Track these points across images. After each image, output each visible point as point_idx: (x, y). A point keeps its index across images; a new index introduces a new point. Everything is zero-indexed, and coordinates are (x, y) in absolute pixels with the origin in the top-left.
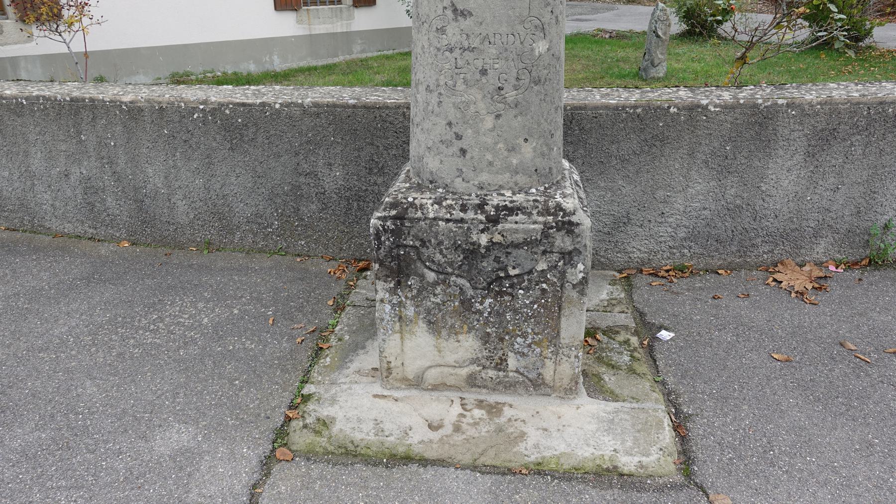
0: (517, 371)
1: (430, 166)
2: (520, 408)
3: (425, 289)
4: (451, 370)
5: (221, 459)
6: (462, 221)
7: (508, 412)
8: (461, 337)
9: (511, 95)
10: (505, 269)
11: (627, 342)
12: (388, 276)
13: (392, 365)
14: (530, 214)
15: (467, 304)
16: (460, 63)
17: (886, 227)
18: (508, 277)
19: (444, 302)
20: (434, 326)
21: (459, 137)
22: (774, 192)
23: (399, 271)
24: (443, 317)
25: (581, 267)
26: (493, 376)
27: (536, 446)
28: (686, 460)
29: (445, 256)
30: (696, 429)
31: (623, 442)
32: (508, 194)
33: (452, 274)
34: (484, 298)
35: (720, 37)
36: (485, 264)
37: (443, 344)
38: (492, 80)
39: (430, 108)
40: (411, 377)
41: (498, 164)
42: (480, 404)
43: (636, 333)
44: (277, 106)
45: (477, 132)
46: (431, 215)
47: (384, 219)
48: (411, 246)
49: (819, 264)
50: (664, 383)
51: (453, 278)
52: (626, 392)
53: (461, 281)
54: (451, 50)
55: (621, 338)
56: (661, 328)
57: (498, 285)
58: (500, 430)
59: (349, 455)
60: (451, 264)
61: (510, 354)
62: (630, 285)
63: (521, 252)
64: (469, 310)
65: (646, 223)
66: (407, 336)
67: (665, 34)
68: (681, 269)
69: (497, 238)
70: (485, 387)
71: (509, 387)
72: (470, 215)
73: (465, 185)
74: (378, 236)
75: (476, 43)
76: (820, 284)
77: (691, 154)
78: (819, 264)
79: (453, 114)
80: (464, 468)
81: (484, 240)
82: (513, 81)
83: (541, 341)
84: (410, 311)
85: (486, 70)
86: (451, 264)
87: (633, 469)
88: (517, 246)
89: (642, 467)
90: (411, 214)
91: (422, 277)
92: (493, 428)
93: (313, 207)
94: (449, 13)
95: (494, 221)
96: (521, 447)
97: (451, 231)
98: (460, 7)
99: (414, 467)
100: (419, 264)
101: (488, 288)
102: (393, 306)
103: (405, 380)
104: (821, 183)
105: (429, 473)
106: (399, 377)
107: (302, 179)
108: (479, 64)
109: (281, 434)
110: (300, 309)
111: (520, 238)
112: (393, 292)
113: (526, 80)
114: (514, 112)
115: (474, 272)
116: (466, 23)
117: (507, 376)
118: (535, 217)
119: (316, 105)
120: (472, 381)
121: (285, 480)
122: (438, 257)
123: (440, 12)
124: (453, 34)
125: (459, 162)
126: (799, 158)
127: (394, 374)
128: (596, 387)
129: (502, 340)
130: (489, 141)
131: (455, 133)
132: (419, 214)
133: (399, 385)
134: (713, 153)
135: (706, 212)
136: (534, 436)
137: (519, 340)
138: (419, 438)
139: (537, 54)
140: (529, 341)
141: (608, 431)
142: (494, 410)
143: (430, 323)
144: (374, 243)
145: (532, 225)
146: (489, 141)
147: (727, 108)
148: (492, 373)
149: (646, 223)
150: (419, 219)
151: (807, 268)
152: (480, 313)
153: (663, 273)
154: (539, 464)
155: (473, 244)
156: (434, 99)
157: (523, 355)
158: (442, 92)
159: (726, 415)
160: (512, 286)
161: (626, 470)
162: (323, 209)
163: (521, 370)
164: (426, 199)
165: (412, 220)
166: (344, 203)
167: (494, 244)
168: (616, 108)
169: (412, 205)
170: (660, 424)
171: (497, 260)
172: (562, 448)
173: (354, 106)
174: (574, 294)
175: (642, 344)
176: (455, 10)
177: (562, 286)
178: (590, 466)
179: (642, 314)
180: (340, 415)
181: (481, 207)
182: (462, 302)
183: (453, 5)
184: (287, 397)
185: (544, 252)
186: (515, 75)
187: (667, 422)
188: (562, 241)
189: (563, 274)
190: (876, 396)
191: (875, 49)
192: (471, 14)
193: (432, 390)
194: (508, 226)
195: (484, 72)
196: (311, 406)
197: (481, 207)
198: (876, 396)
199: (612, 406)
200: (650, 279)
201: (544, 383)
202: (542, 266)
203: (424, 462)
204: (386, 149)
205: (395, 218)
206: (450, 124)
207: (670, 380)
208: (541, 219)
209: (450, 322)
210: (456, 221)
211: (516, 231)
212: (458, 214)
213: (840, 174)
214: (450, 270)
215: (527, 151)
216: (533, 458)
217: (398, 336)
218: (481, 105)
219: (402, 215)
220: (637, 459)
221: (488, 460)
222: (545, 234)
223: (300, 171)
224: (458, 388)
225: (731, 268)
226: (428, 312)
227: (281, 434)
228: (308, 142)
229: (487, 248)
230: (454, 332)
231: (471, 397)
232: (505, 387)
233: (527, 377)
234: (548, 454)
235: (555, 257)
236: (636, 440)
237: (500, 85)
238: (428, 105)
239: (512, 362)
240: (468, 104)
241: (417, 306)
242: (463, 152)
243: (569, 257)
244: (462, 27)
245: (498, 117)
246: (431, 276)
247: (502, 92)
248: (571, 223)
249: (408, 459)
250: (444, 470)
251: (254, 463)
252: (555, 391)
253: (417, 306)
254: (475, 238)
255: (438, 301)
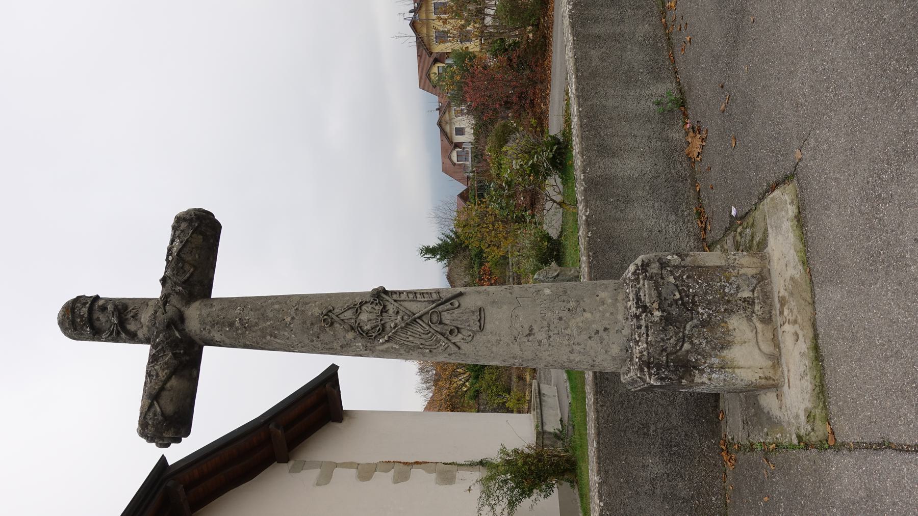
0: (753, 291)
1: (617, 351)
2: (779, 287)
3: (696, 349)
4: (760, 335)
5: (841, 485)
6: (647, 327)
7: (783, 293)
8: (731, 328)
9: (572, 304)
10: (676, 301)
11: (740, 234)
12: (690, 375)
13: (762, 375)
14: (639, 289)
15: (704, 324)
16: (556, 332)
17: (658, 104)
18: (681, 299)
19: (705, 338)
20: (725, 345)
21: (597, 332)
22: (639, 169)
23: (686, 367)
24: (717, 339)
25: (669, 257)
26: (761, 305)
27: (795, 267)
28: (786, 179)
29: (671, 337)
30: (772, 178)
31: (783, 217)
32: (629, 303)
33: (683, 332)
34: (698, 313)
35: (560, 236)
36: (674, 313)
37: (738, 339)
38: (564, 314)
40: (771, 363)
41: (611, 310)
42: (781, 313)
43: (736, 230)
44: (602, 504)
45: (594, 322)
46: (645, 345)
47: (650, 375)
48: (667, 358)
49: (687, 133)
50: (756, 204)
51: (687, 332)
52: (763, 224)
53: (688, 327)
54: (550, 337)
55: (738, 238)
56: (731, 216)
57: (688, 305)
58: (791, 294)
59: (821, 391)
60: (677, 334)
61: (739, 295)
63: (663, 291)
64: (709, 322)
65: (667, 240)
66: (735, 363)
67: (556, 270)
68: (699, 214)
69: (656, 305)
70: (770, 312)
71: (766, 296)
72: (643, 322)
73: (626, 328)
74: (662, 379)
75: (545, 323)
76: (696, 130)
77: (617, 220)
78: (687, 133)
79: (584, 336)
80: (815, 309)
81: (658, 314)
83: (725, 277)
84: (715, 361)
86: (677, 334)
87: (795, 207)
88: (660, 294)
89: (792, 202)
90: (645, 358)
91: (688, 352)
92: (791, 299)
93: (680, 485)
94: (531, 338)
95: (645, 308)
96: (797, 277)
97: (654, 333)
98: (528, 332)
99: (820, 341)
100: (679, 354)
101: (691, 311)
102: (713, 372)
103: (773, 366)
105: (821, 330)
106: (772, 372)
107: (658, 491)
108: (556, 321)
109: (821, 446)
110: (756, 479)
111: (654, 293)
112: (702, 372)
113: (565, 298)
115: (680, 319)
117: (758, 298)
118: (641, 285)
119: (599, 473)
120: (767, 320)
121: (847, 432)
122: (672, 341)
123: (530, 344)
124: (541, 336)
125: (612, 332)
126: (616, 160)
127: (771, 375)
128: (763, 244)
129: (729, 301)
130: (598, 315)
132: (645, 353)
133: (779, 373)
134: (616, 208)
135: (656, 205)
136: (791, 272)
137: (727, 290)
138: (804, 346)
140: (727, 284)
141: (780, 227)
142: (783, 302)
143: (722, 348)
144: (667, 382)
145: (646, 287)
146: (598, 315)
147: (587, 204)
148: (757, 307)
149: (667, 240)
150: (648, 353)
151: (690, 140)
152: (709, 315)
153: (703, 225)
154: (803, 263)
155: (661, 320)
156: (577, 348)
157: (738, 287)
159: (764, 164)
160: (688, 296)
161: (796, 211)
162: (681, 477)
163: (751, 288)
164: (637, 350)
165: (649, 358)
166: (674, 458)
167: (660, 307)
168: (590, 267)
169: (640, 358)
170: (772, 199)
171: (670, 305)
172: (792, 251)
173: (598, 443)
174: (688, 259)
175: (740, 224)
176: (530, 335)
177: (684, 267)
178: (798, 232)
179: (727, 230)
180: (803, 407)
181: (638, 317)
182: (703, 327)
184: (803, 454)
185: (662, 278)
187: (771, 196)
188: (654, 269)
189: (675, 267)
190: (743, 89)
191: (565, 131)
193: (779, 348)
194: (647, 300)
195: (560, 319)
196: (802, 432)
197: (638, 317)
198: (743, 89)
199: (770, 230)
200: (708, 232)
201: (760, 274)
202: (671, 279)
203: (816, 337)
204: (628, 421)
205: (649, 368)
207: (754, 201)
208: (641, 282)
209: (719, 334)
210: (647, 330)
211: (650, 295)
212: (643, 329)
213: (624, 137)
214: (681, 334)
215: (603, 295)
216: (801, 268)
217: (736, 370)
218: (578, 320)
219: (647, 364)
220: (789, 206)
221: (808, 296)
222: (651, 278)
223: (651, 492)
224: (775, 330)
225: (694, 184)
226: (714, 348)
227: (821, 446)
228: (628, 483)
229: (663, 311)
230: (727, 332)
231: (779, 320)
232: (768, 298)
233: (757, 285)
234: (797, 259)
235: (664, 272)
236: (782, 210)
239: (746, 294)
240: (578, 327)
241: (711, 356)
242: (606, 329)
243: (663, 264)
245: (584, 310)
246: (687, 346)
248: (642, 265)
249: (816, 348)
250: (818, 321)
251: (838, 457)
252: (765, 267)
253: (711, 356)
254: (657, 319)
255: (704, 342)
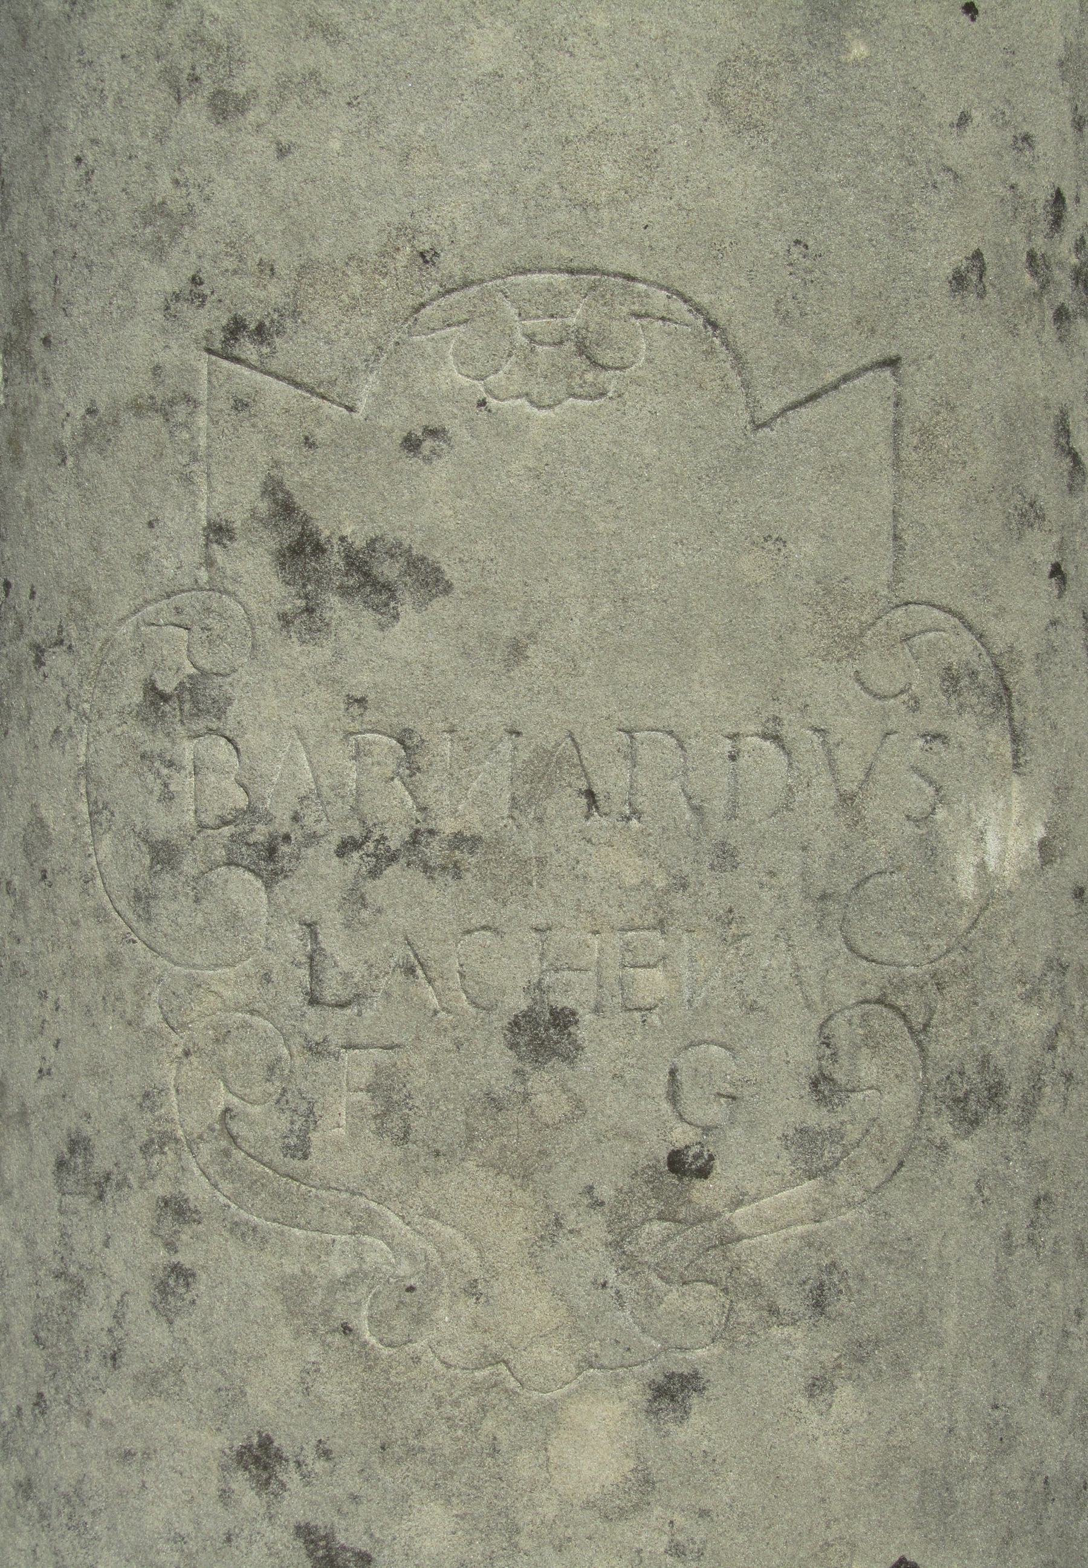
9: (766, 1205)
39: (94, 1319)
54: (270, 859)
62: (168, 215)
75: (469, 796)
82: (793, 1107)
85: (563, 1019)
94: (254, 570)
98: (342, 522)
104: (262, 703)
113: (885, 1091)
114: (799, 1345)
116: (395, 649)
131: (305, 1533)
139: (967, 885)
158: (197, 1189)
176: (301, 551)
183: (285, 508)
186: (802, 1052)
192: (430, 580)
206: (260, 1458)
218: (529, 1306)
237: (681, 1136)
238: (78, 1289)
244: (362, 682)
245: (672, 1392)
247: (703, 1193)
